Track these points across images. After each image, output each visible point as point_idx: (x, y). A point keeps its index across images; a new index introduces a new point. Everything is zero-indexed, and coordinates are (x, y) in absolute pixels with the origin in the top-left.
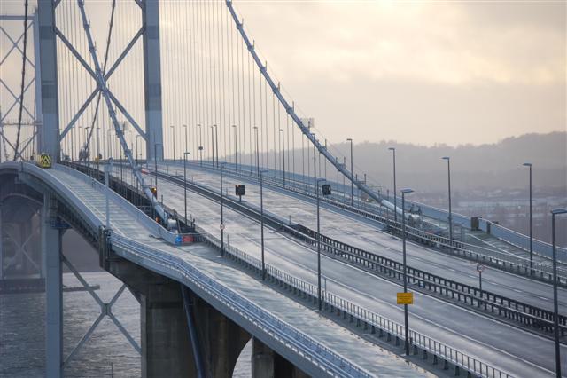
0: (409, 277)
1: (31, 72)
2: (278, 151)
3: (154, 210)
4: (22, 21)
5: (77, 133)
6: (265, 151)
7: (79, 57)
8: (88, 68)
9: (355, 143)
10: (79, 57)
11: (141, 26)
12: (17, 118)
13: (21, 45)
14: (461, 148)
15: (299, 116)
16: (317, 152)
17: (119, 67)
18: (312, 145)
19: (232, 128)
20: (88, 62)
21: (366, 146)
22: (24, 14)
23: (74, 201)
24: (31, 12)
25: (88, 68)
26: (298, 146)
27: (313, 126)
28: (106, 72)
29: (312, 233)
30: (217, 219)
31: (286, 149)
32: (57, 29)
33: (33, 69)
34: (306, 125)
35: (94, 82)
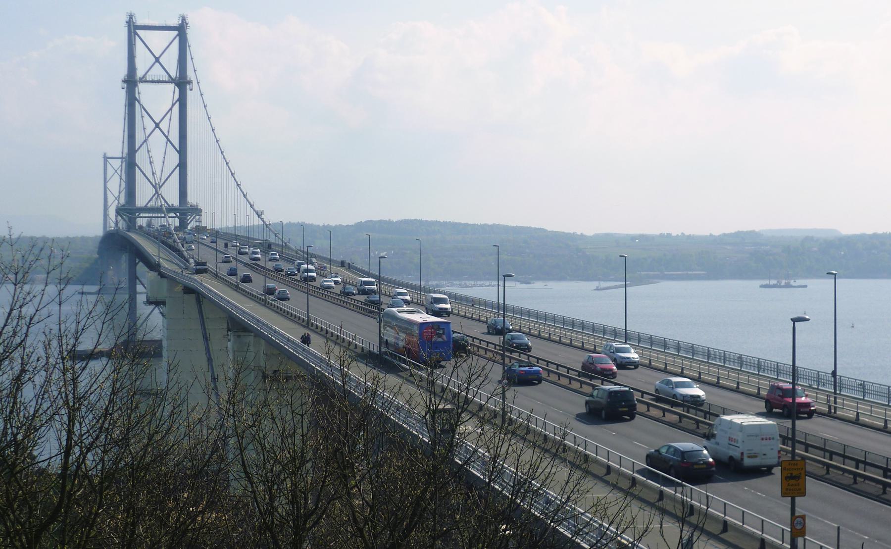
0: (310, 289)
1: (123, 185)
2: (245, 226)
3: (182, 254)
4: (116, 173)
5: (230, 221)
6: (252, 224)
7: (147, 178)
8: (151, 183)
9: (284, 223)
10: (147, 178)
11: (178, 162)
12: (54, 297)
13: (119, 172)
14: (336, 226)
15: (256, 209)
16: (265, 227)
17: (165, 184)
18: (262, 223)
19: (233, 215)
20: (151, 181)
21: (290, 225)
22: (120, 160)
23: (152, 260)
24: (125, 155)
25: (151, 183)
26: (256, 223)
27: (263, 214)
28: (161, 184)
29: (262, 267)
30: (492, 382)
31: (250, 225)
32: (136, 164)
33: (124, 183)
34: (260, 214)
35: (154, 190)
